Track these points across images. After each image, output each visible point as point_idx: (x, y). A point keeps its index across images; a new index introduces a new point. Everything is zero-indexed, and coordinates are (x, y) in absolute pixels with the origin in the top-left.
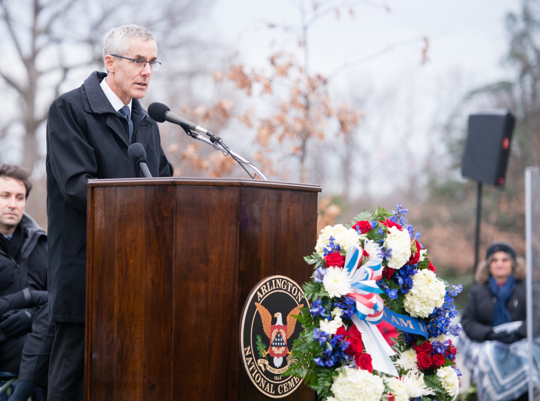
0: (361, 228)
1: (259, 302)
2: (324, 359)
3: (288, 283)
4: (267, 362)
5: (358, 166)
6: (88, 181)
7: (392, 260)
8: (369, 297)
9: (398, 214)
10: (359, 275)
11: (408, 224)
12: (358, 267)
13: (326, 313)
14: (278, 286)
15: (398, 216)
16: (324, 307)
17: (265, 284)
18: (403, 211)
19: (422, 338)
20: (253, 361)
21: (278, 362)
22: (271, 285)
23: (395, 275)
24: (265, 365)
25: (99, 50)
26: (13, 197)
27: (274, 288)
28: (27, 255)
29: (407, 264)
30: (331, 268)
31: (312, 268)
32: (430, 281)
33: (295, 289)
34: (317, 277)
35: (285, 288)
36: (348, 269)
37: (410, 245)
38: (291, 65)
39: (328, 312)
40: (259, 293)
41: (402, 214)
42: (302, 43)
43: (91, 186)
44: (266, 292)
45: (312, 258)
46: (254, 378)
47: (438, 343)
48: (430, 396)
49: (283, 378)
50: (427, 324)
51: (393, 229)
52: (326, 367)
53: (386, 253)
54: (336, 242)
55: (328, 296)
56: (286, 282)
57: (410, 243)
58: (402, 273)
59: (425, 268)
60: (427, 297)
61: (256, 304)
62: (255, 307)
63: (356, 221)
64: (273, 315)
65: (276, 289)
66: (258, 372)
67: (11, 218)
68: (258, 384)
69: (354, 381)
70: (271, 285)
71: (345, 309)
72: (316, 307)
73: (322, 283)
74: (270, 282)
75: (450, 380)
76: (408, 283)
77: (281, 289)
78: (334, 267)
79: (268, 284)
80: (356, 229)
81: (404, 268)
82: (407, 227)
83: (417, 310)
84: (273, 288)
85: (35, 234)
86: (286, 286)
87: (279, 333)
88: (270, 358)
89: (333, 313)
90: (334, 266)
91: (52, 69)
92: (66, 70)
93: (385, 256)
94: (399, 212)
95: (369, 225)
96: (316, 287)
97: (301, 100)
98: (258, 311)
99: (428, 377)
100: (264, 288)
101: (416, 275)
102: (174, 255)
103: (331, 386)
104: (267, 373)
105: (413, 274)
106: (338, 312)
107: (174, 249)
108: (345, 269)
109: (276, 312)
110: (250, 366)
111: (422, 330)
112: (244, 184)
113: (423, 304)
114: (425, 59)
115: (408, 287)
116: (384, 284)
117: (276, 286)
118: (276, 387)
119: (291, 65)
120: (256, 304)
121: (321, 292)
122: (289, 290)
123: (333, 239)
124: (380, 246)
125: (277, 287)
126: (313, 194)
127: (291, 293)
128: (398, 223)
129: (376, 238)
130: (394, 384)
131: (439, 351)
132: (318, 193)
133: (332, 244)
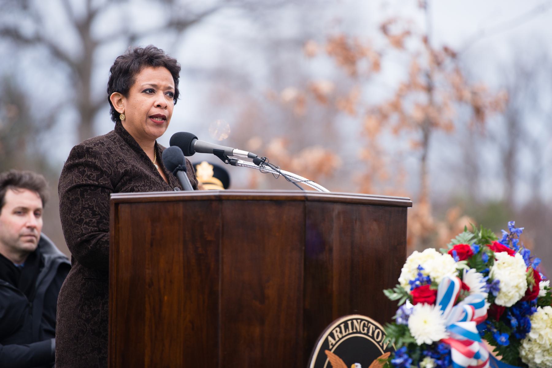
1: (330, 350)
3: (370, 324)
6: (111, 196)
7: (501, 295)
8: (468, 343)
9: (510, 235)
11: (524, 248)
12: (456, 303)
14: (356, 329)
15: (511, 237)
16: (410, 356)
17: (339, 326)
18: (517, 231)
22: (346, 327)
26: (31, 214)
27: (351, 331)
28: (43, 289)
31: (395, 306)
33: (378, 333)
34: (401, 317)
35: (366, 331)
36: (441, 307)
37: (526, 275)
38: (408, 33)
39: (416, 363)
40: (330, 339)
41: (515, 234)
43: (114, 202)
44: (340, 336)
45: (395, 292)
51: (502, 256)
54: (425, 273)
55: (415, 342)
56: (366, 323)
57: (526, 273)
58: (517, 312)
59: (548, 305)
60: (550, 343)
61: (327, 352)
62: (326, 357)
63: (454, 244)
65: (353, 333)
67: (31, 241)
70: (346, 327)
71: (438, 359)
72: (400, 356)
73: (407, 326)
74: (346, 323)
76: (525, 325)
77: (360, 333)
78: (423, 304)
79: (342, 326)
80: (452, 255)
81: (518, 304)
82: (523, 251)
84: (349, 331)
85: (53, 262)
86: (366, 329)
90: (423, 303)
91: (112, 38)
93: (492, 289)
94: (511, 233)
96: (400, 331)
97: (422, 80)
98: (329, 363)
100: (337, 331)
101: (535, 314)
102: (220, 289)
107: (220, 283)
108: (438, 307)
109: (354, 363)
112: (309, 198)
113: (545, 353)
116: (492, 326)
117: (353, 329)
119: (408, 33)
120: (327, 352)
121: (406, 337)
122: (370, 334)
124: (485, 276)
125: (355, 331)
126: (401, 209)
127: (373, 337)
128: (510, 246)
129: (480, 266)
132: (408, 208)
133: (420, 275)
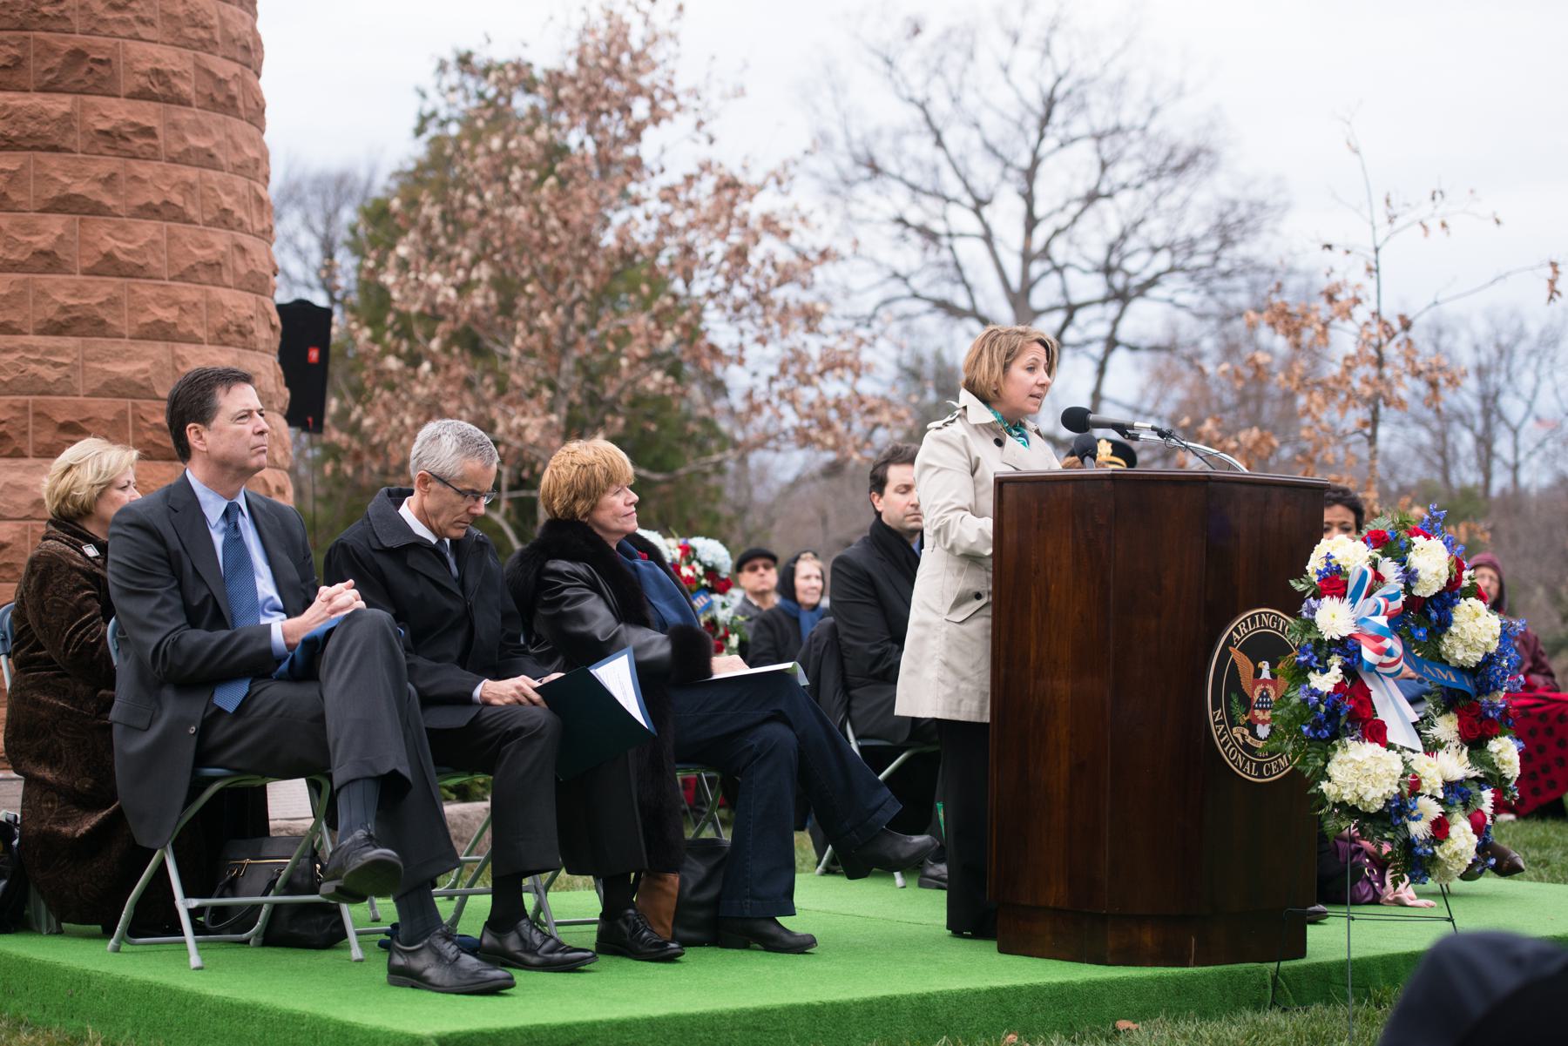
0: (1373, 540)
2: (1316, 727)
4: (1246, 732)
5: (1503, 446)
10: (1365, 606)
13: (1318, 662)
17: (1245, 620)
19: (1465, 694)
20: (1225, 729)
21: (1263, 731)
22: (1253, 621)
23: (1425, 606)
24: (1243, 736)
25: (1119, 280)
29: (1444, 589)
30: (1327, 598)
31: (1300, 597)
32: (1477, 615)
42: (1372, 270)
46: (1227, 754)
47: (1491, 703)
48: (1476, 778)
49: (1271, 754)
50: (1475, 677)
52: (1319, 739)
53: (1410, 577)
58: (1437, 604)
64: (1256, 665)
66: (1233, 745)
68: (1233, 762)
69: (1359, 759)
70: (1253, 621)
72: (1305, 654)
73: (1313, 620)
74: (1252, 617)
75: (1506, 756)
81: (1439, 595)
83: (1459, 657)
87: (1265, 690)
88: (1252, 727)
89: (1330, 661)
92: (1071, 309)
95: (1385, 536)
99: (1474, 752)
103: (1326, 766)
104: (1247, 747)
105: (1453, 605)
106: (1335, 662)
110: (1220, 737)
111: (1467, 685)
114: (1553, 293)
115: (1445, 623)
118: (1259, 766)
123: (1332, 557)
127: (1283, 633)
130: (1421, 763)
131: (1491, 714)
133: (1328, 564)
